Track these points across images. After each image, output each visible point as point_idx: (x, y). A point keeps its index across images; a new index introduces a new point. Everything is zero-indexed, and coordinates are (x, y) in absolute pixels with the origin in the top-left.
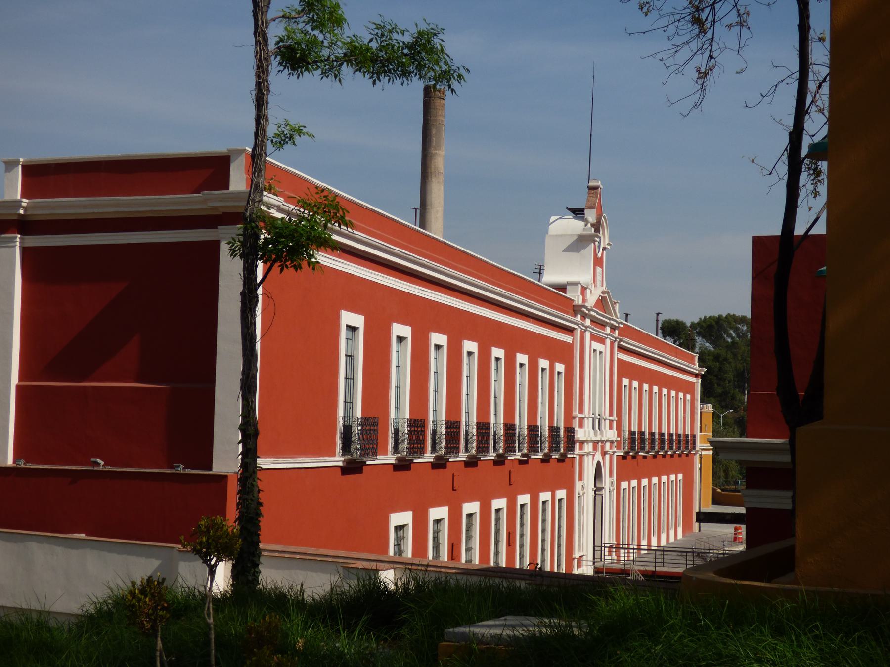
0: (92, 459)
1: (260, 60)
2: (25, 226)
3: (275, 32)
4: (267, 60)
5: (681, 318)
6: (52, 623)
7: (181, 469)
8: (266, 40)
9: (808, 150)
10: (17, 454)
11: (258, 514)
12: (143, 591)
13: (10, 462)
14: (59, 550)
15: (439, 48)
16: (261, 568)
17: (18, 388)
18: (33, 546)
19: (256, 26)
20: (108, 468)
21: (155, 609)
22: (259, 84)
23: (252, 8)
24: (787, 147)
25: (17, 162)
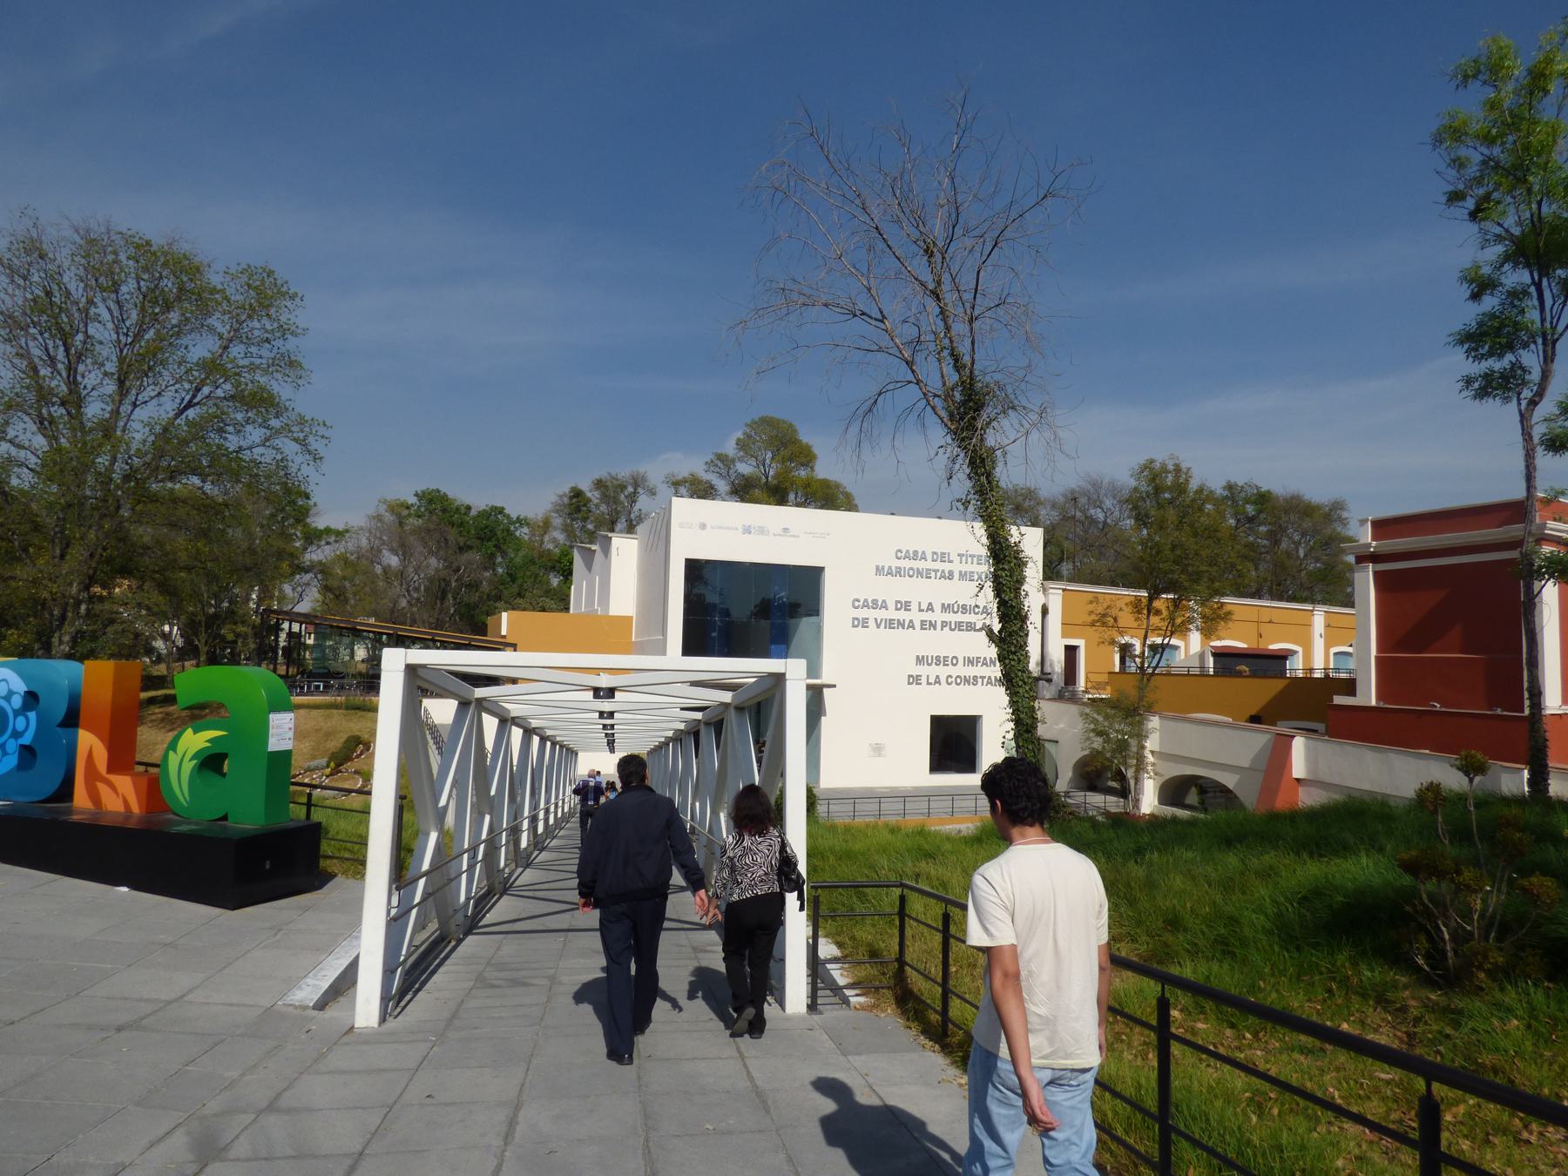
1: (1527, 451)
2: (1375, 558)
3: (1538, 431)
4: (1533, 450)
5: (636, 752)
6: (1392, 803)
7: (1499, 711)
8: (1531, 438)
10: (1379, 698)
11: (1546, 747)
12: (1427, 789)
13: (1373, 703)
14: (1411, 759)
16: (1549, 781)
17: (1377, 658)
18: (1392, 756)
19: (1523, 429)
20: (1443, 709)
21: (1436, 798)
22: (1527, 467)
23: (1519, 418)
24: (178, 815)
25: (1367, 520)
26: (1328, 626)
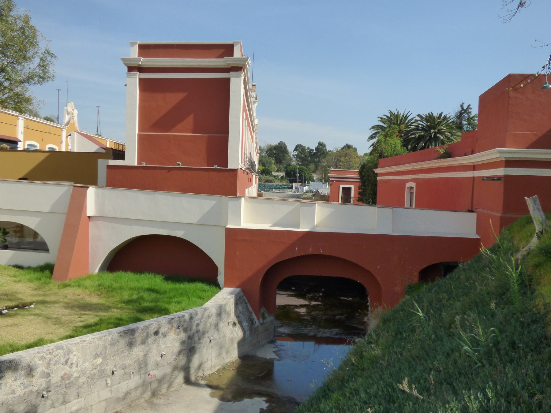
0: (177, 163)
2: (141, 69)
7: (216, 167)
9: (245, 399)
13: (136, 165)
15: (372, 147)
26: (26, 127)
